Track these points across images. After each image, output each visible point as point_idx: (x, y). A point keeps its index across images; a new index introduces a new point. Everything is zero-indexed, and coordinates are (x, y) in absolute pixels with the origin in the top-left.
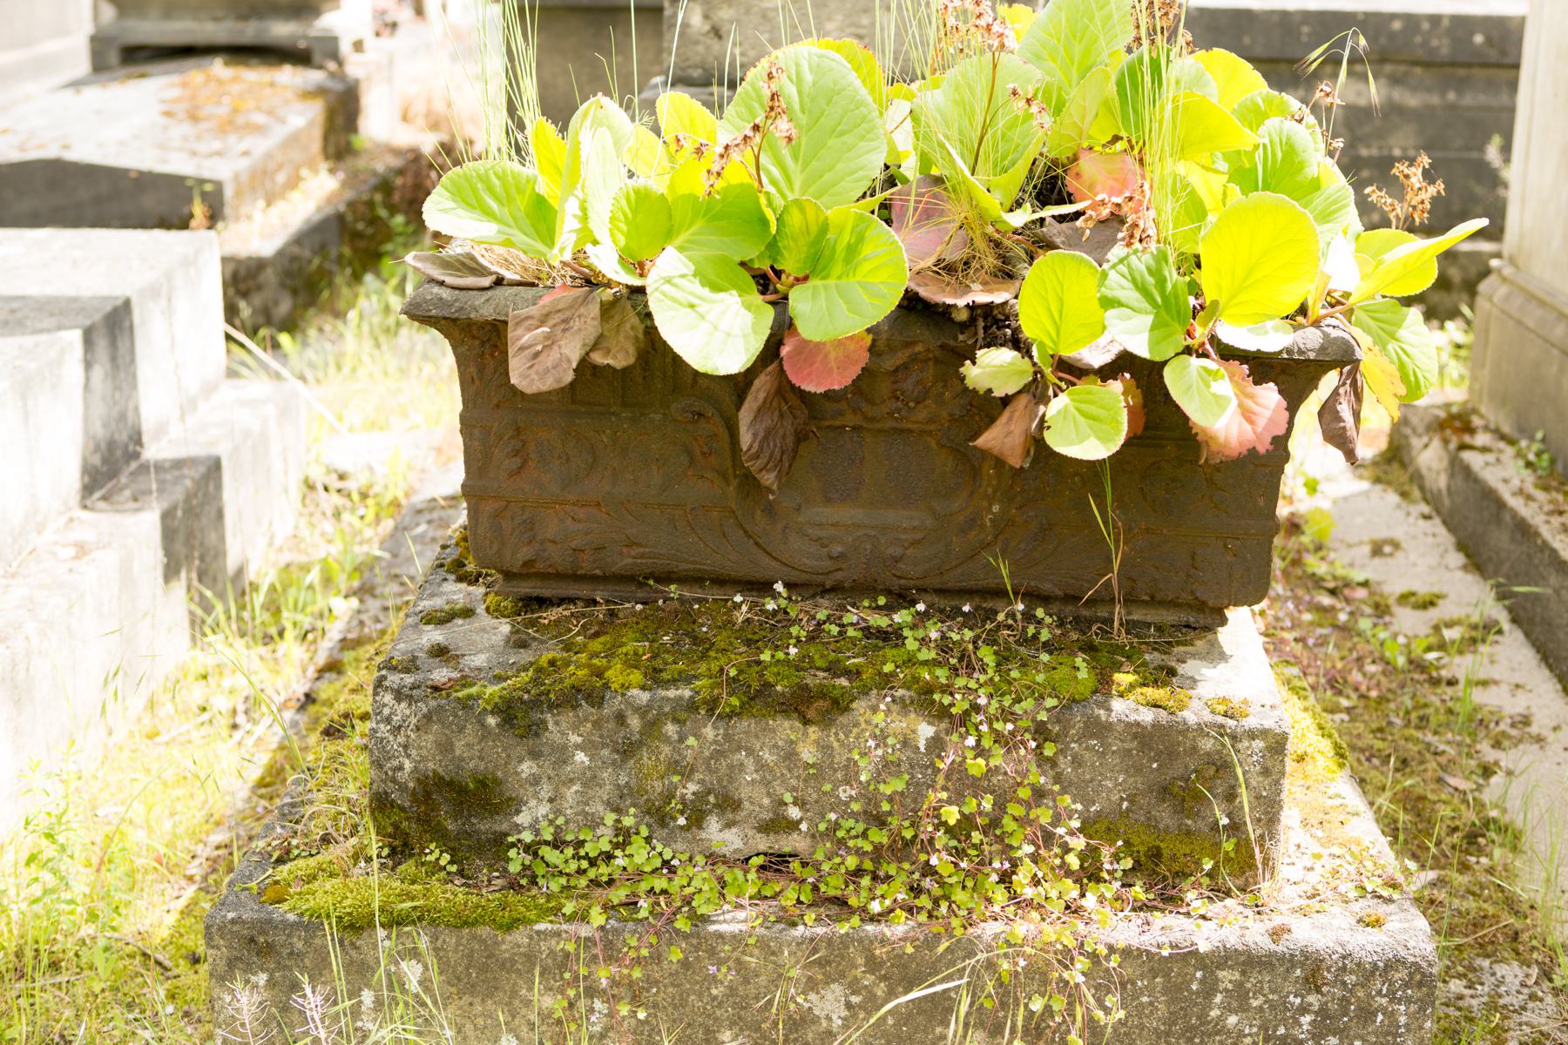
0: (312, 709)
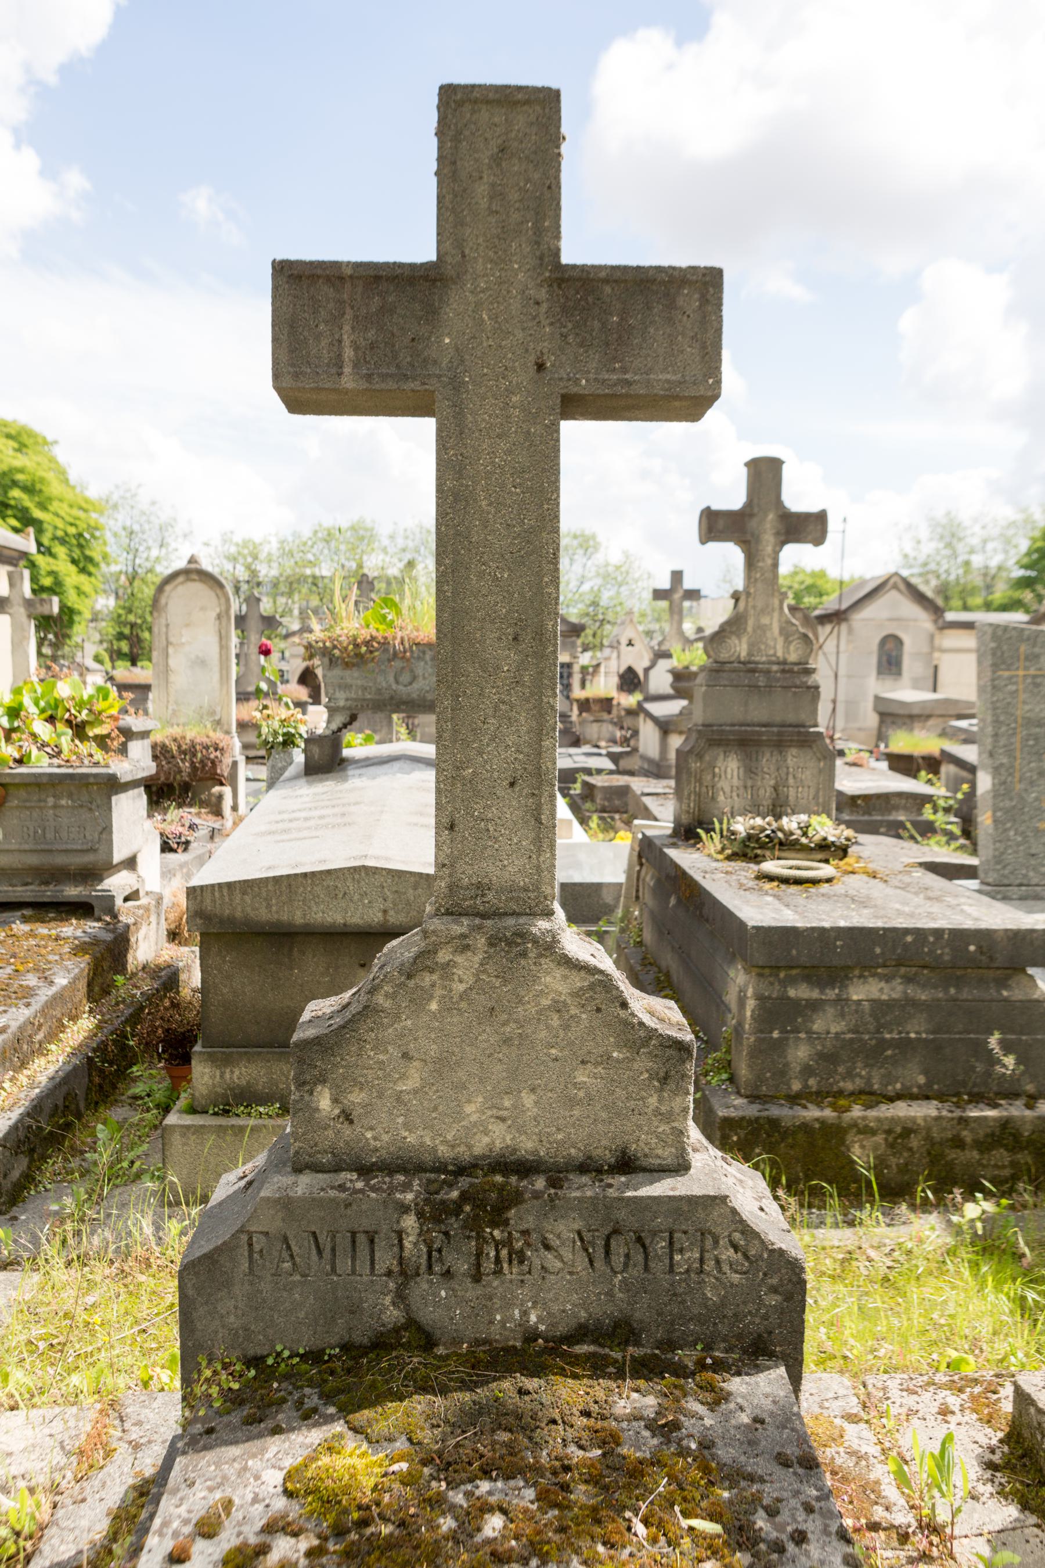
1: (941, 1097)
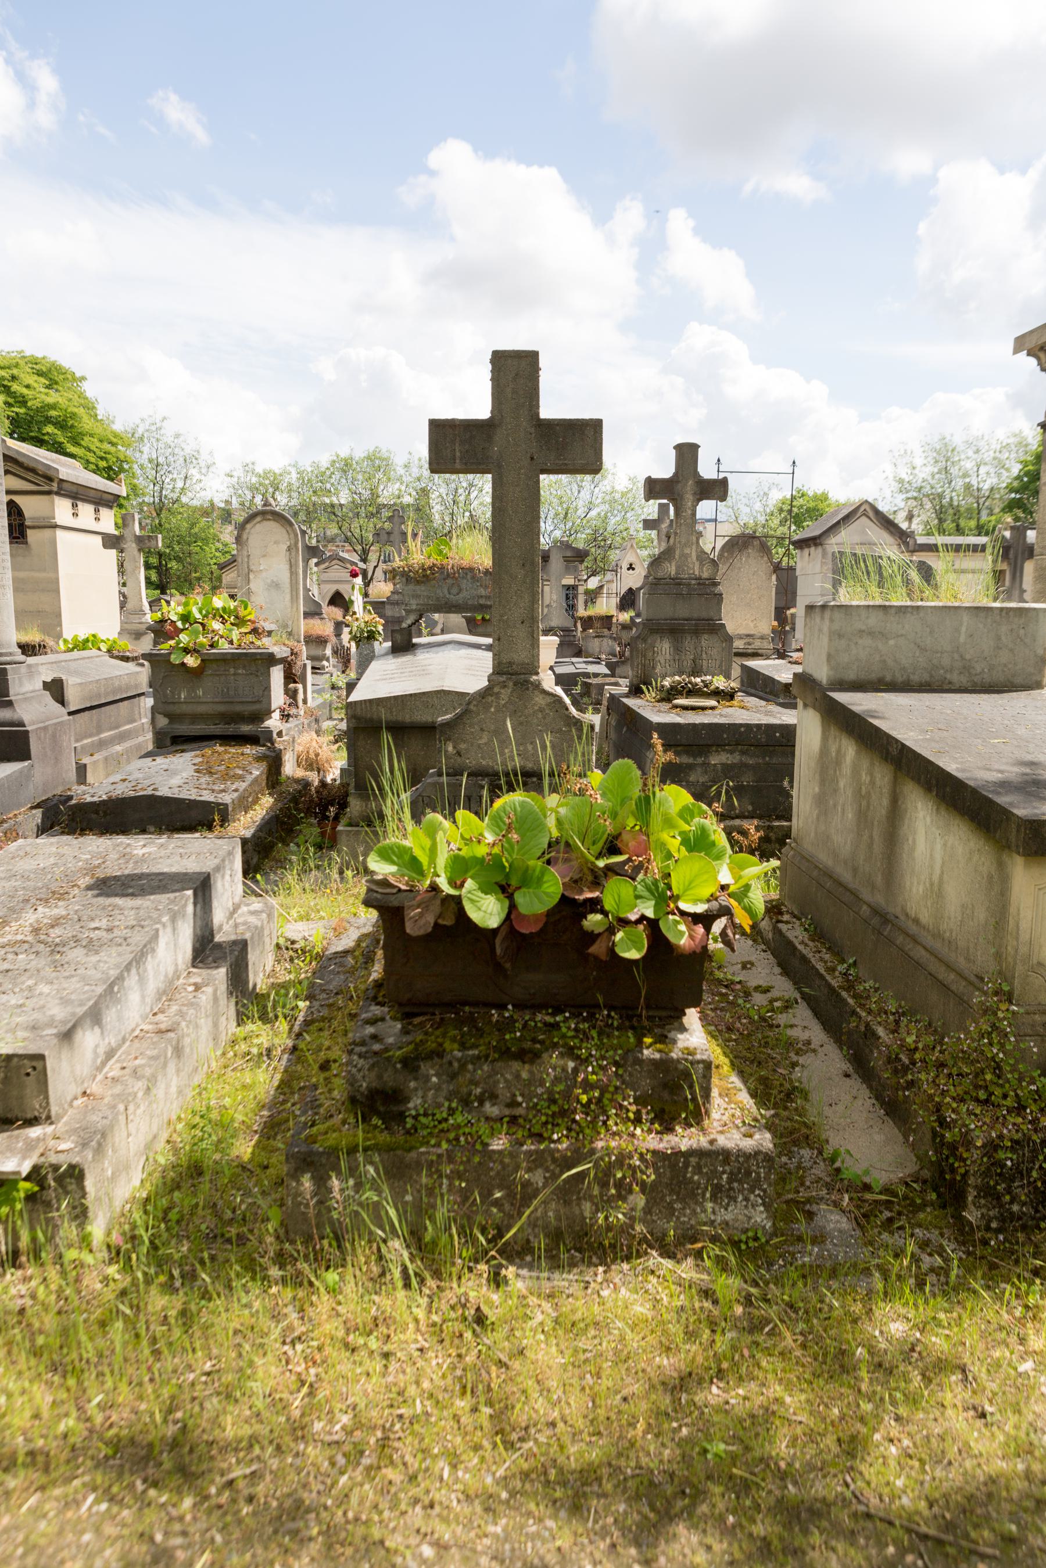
0: (297, 1053)
1: (760, 817)
